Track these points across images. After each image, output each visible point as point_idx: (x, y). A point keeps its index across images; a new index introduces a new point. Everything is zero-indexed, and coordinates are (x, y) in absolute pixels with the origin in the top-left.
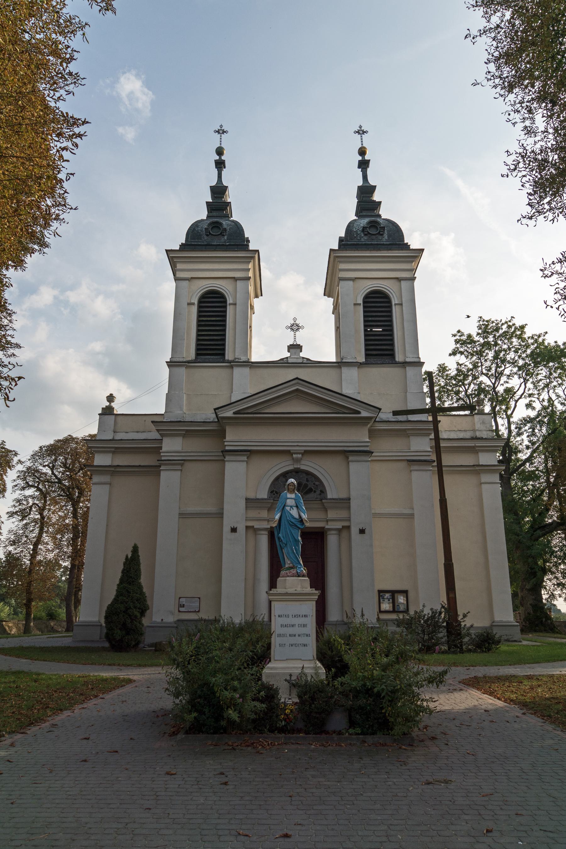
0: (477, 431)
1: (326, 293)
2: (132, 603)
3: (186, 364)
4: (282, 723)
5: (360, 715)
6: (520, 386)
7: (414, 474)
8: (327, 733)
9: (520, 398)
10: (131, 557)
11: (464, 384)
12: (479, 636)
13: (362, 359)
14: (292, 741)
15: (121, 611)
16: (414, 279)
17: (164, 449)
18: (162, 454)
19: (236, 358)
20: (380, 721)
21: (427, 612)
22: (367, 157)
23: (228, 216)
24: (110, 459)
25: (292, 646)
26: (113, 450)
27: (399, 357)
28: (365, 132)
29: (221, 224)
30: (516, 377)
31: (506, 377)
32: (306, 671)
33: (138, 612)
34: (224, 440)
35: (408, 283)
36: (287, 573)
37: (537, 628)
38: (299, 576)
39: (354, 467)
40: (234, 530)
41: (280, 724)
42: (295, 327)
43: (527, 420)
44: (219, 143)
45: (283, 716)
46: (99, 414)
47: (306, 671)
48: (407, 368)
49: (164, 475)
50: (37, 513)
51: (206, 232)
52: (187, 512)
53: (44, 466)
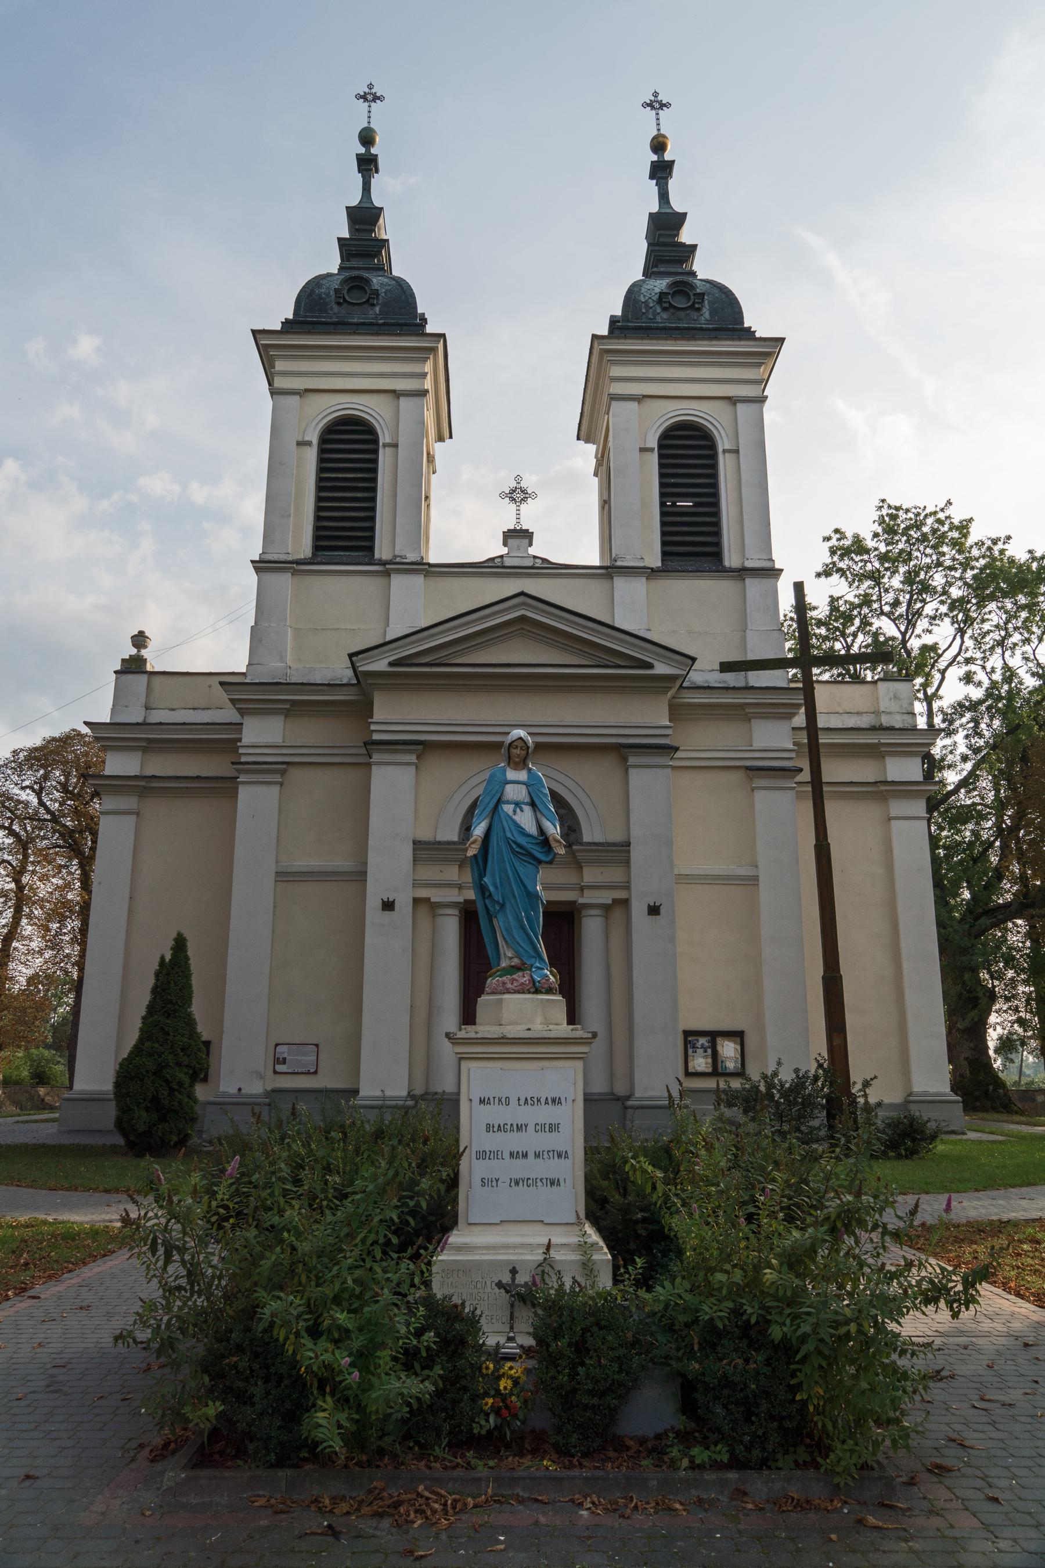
0: (883, 714)
1: (582, 433)
2: (170, 1056)
3: (293, 566)
4: (487, 1421)
5: (725, 1406)
6: (954, 639)
7: (759, 795)
8: (619, 1445)
9: (950, 665)
10: (171, 960)
11: (843, 635)
12: (893, 1124)
13: (656, 562)
14: (518, 1491)
15: (147, 1071)
16: (762, 400)
17: (245, 741)
18: (241, 751)
19: (395, 556)
20: (788, 1424)
21: (787, 1076)
22: (668, 156)
23: (384, 269)
24: (139, 762)
25: (517, 1183)
26: (145, 744)
27: (731, 559)
28: (665, 105)
29: (368, 281)
30: (947, 620)
31: (927, 619)
32: (558, 1258)
33: (185, 1074)
34: (370, 720)
35: (753, 407)
36: (504, 983)
37: (978, 1104)
38: (537, 991)
39: (638, 778)
40: (388, 906)
41: (481, 1426)
42: (518, 495)
43: (961, 707)
44: (366, 120)
45: (491, 1401)
46: (115, 672)
47: (556, 1255)
48: (748, 581)
49: (244, 793)
50: (8, 879)
51: (337, 297)
52: (293, 870)
53: (23, 788)
